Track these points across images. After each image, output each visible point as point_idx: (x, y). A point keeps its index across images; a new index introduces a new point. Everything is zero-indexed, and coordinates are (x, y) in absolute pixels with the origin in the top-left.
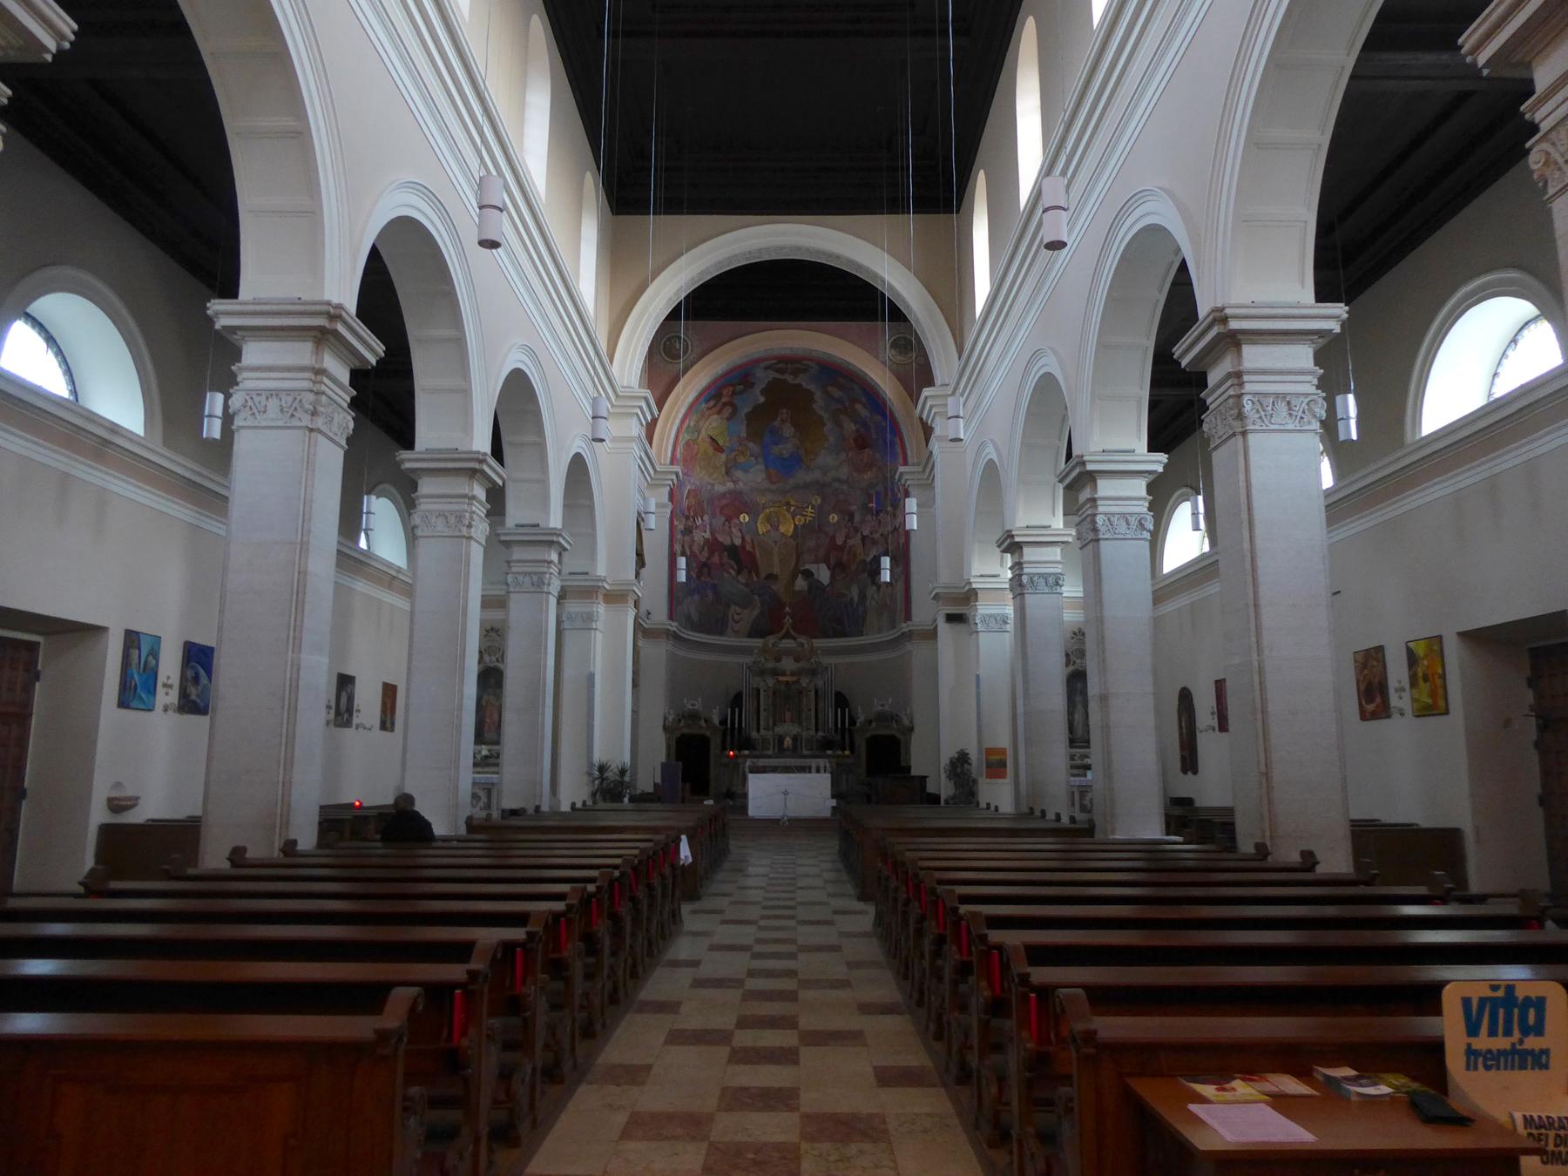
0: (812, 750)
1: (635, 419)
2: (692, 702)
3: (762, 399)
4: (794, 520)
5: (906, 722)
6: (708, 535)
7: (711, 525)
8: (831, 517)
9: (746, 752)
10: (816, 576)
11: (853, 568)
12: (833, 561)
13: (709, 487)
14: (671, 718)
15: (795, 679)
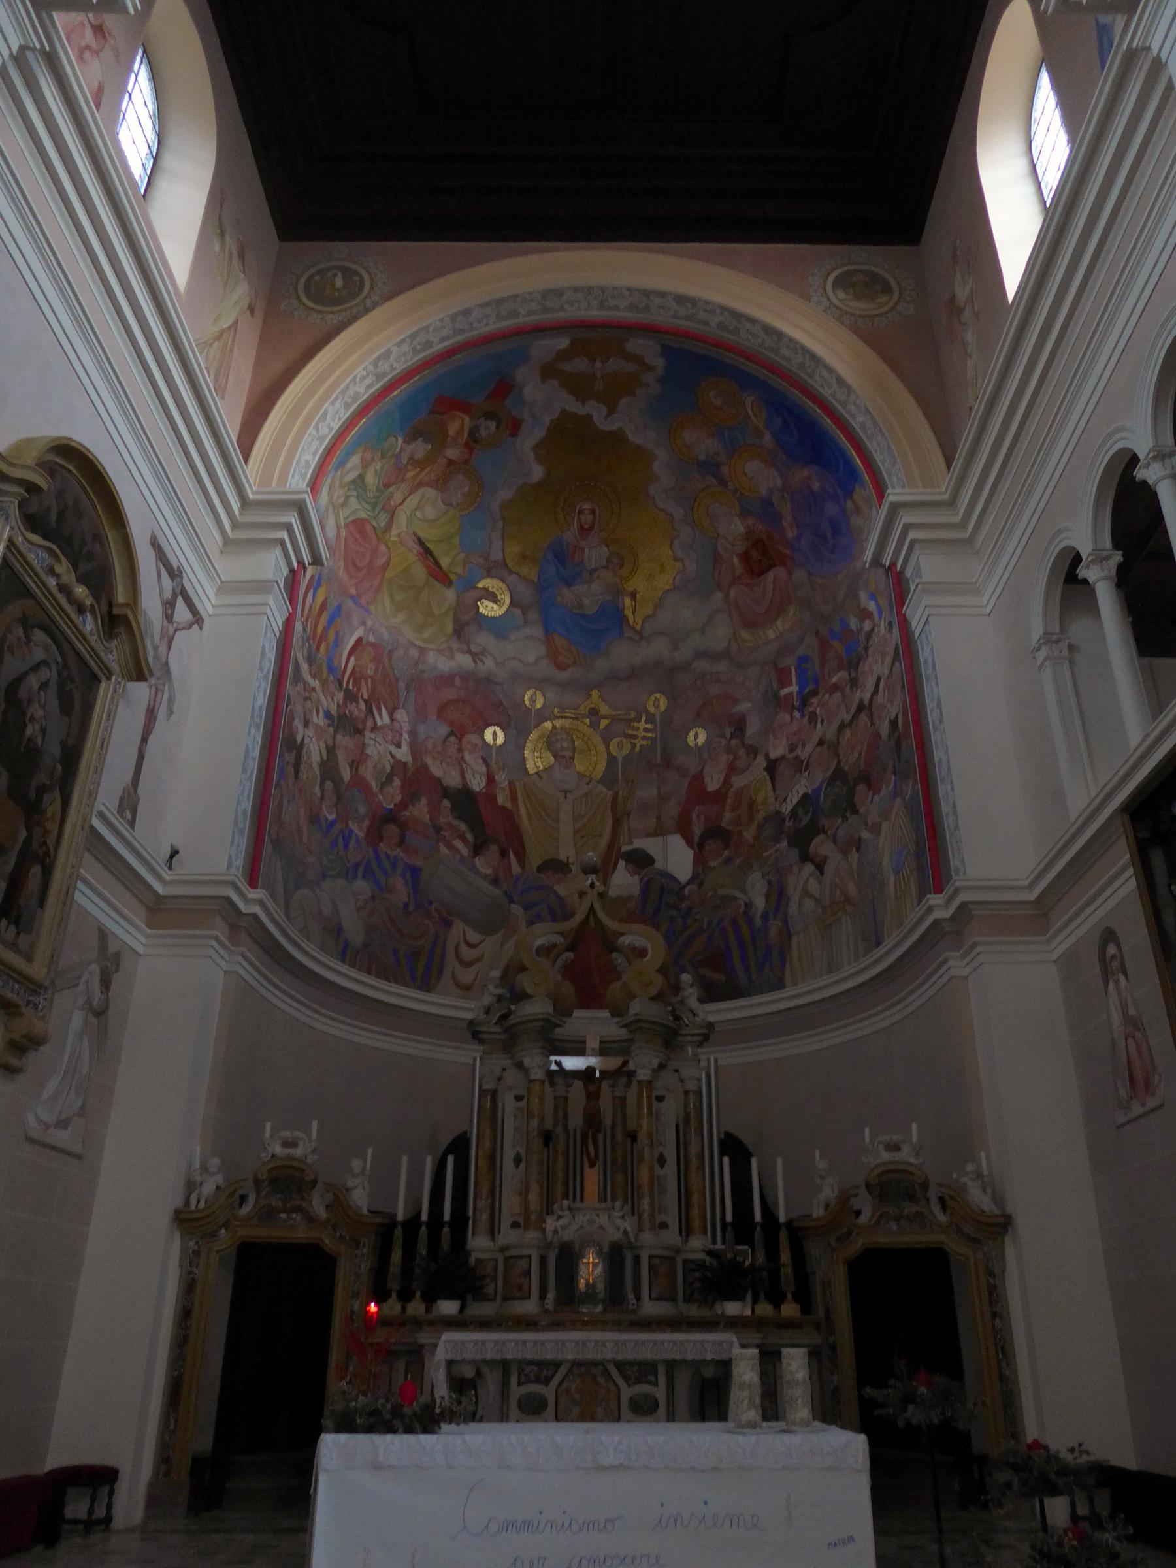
0: (673, 1300)
1: (278, 551)
2: (287, 1134)
3: (537, 472)
4: (607, 746)
5: (978, 1198)
6: (403, 753)
7: (413, 733)
8: (691, 734)
9: (449, 1307)
10: (659, 865)
11: (749, 835)
12: (697, 829)
13: (414, 653)
14: (208, 1188)
15: (614, 1063)
